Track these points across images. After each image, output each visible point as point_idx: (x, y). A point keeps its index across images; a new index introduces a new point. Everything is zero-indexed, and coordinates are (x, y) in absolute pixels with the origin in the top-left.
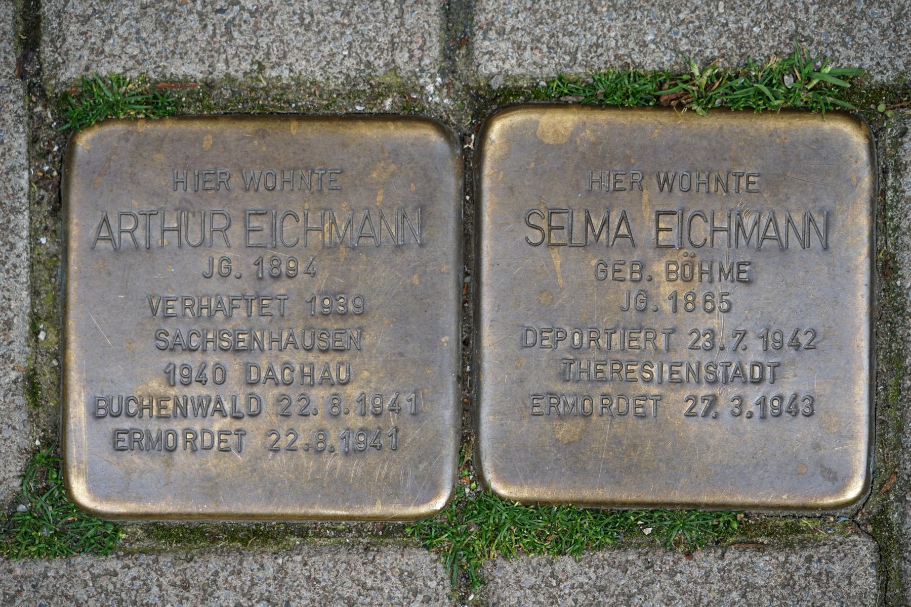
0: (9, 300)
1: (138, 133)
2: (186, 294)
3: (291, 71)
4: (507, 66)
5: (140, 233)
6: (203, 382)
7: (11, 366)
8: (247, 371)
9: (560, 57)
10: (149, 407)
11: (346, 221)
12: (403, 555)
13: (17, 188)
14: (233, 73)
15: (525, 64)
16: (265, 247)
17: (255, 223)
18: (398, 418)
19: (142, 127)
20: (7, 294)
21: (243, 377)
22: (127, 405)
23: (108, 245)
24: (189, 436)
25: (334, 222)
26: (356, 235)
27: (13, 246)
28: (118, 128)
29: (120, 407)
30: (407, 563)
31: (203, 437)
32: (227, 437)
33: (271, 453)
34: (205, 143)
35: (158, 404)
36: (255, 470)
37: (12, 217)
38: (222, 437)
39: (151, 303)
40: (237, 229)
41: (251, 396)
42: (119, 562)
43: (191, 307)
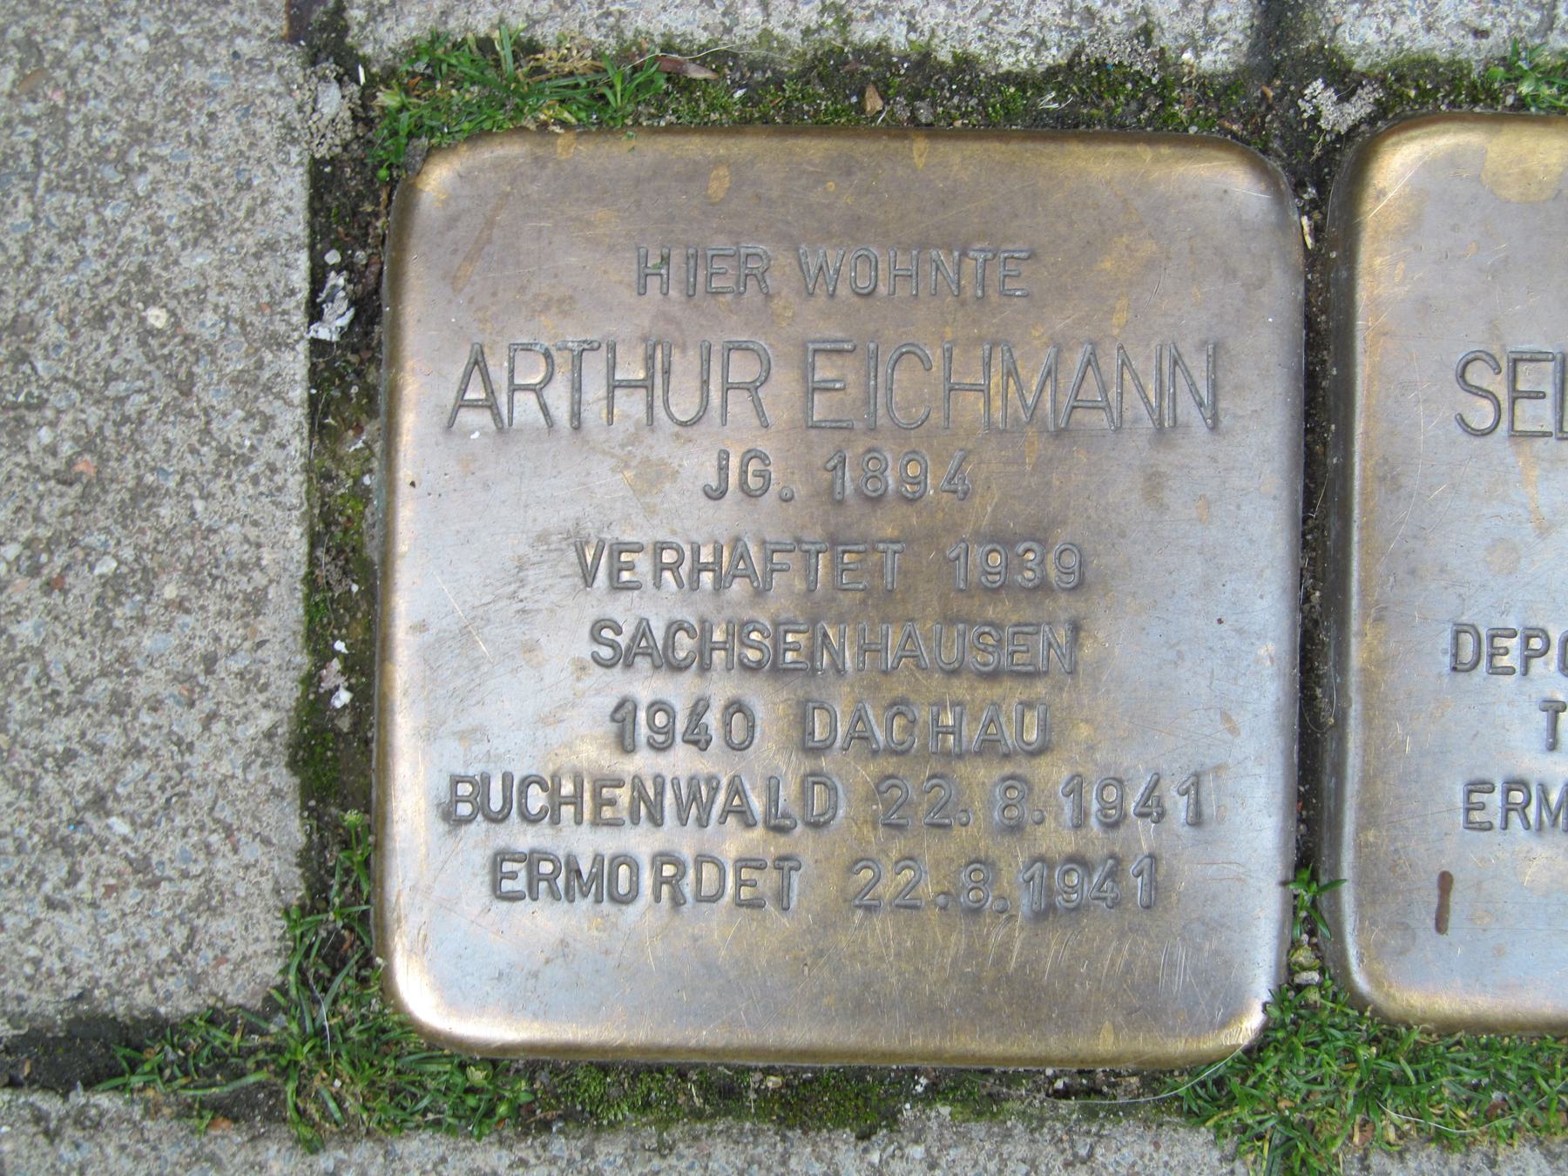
0: (259, 546)
1: (559, 163)
2: (662, 535)
3: (912, 27)
4: (1401, 29)
5: (559, 397)
6: (699, 741)
7: (262, 698)
8: (803, 721)
9: (1519, 13)
10: (576, 800)
11: (1042, 369)
12: (1157, 1145)
13: (280, 289)
14: (778, 31)
15: (1442, 25)
16: (851, 429)
17: (825, 370)
18: (1158, 833)
19: (566, 148)
20: (253, 533)
21: (795, 734)
22: (523, 793)
23: (484, 418)
24: (668, 870)
25: (1011, 372)
26: (1065, 401)
27: (268, 423)
28: (512, 150)
29: (507, 800)
30: (1166, 1164)
31: (699, 872)
32: (755, 875)
33: (860, 913)
34: (714, 185)
35: (596, 794)
36: (821, 953)
37: (268, 357)
38: (745, 874)
39: (581, 556)
40: (784, 383)
41: (813, 778)
42: (504, 1152)
43: (674, 568)
